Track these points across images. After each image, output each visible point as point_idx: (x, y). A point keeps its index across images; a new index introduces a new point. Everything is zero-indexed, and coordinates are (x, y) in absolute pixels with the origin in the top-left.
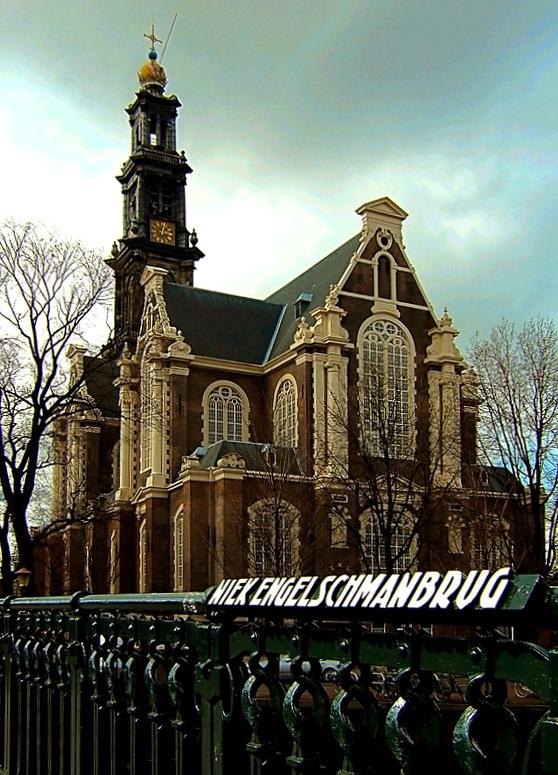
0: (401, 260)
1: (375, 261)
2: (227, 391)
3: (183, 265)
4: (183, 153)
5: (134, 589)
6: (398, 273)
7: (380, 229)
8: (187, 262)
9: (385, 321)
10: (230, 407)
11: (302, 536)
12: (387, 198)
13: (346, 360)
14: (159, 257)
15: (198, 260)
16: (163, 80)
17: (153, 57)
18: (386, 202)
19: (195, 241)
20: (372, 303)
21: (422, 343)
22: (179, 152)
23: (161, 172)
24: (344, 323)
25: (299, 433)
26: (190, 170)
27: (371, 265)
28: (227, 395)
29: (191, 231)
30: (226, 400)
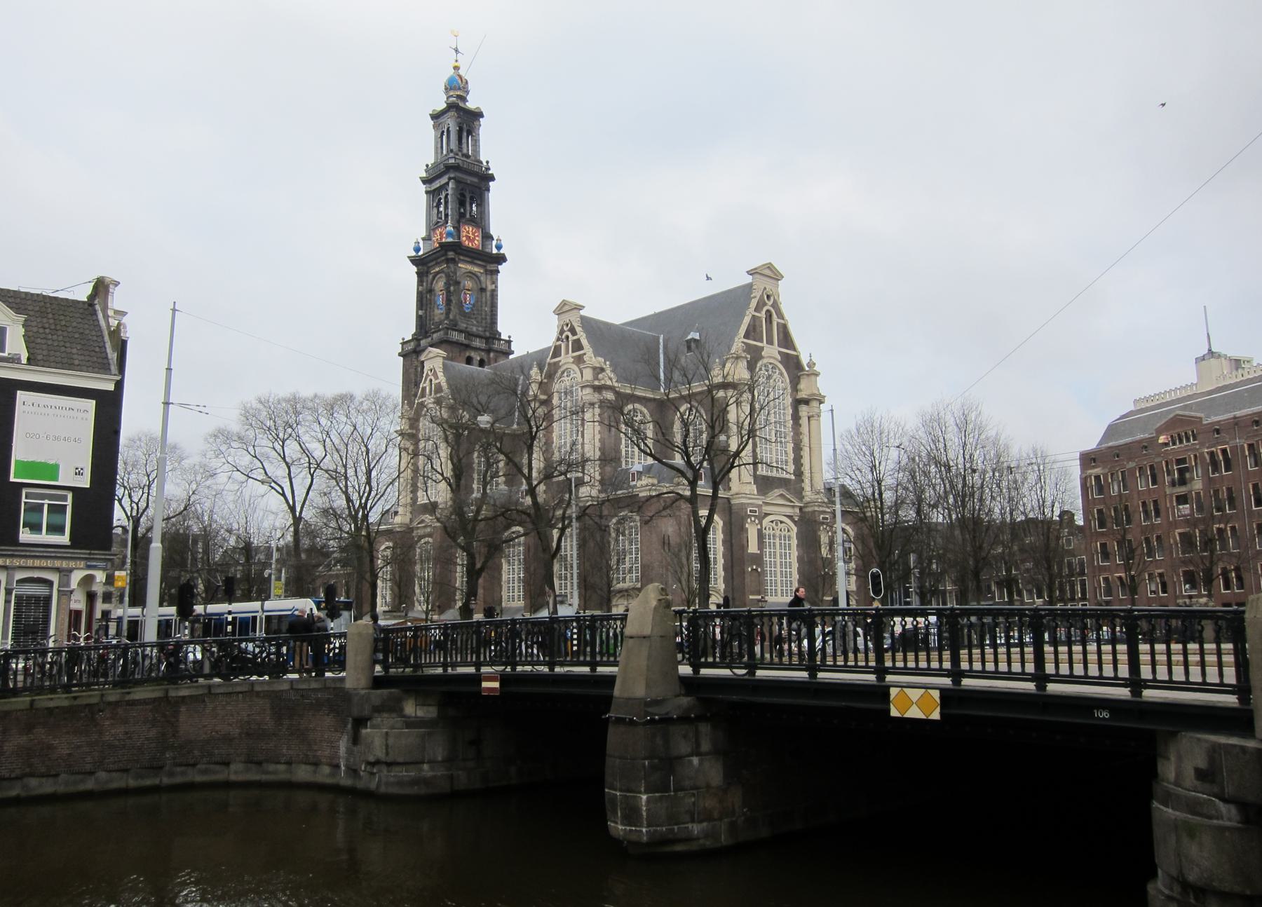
0: (780, 315)
1: (763, 315)
3: (488, 268)
4: (487, 162)
5: (26, 498)
6: (778, 324)
7: (765, 289)
8: (491, 267)
9: (771, 363)
11: (695, 532)
12: (770, 263)
14: (469, 260)
15: (501, 264)
16: (468, 92)
17: (456, 68)
18: (770, 266)
20: (762, 348)
21: (795, 382)
23: (470, 179)
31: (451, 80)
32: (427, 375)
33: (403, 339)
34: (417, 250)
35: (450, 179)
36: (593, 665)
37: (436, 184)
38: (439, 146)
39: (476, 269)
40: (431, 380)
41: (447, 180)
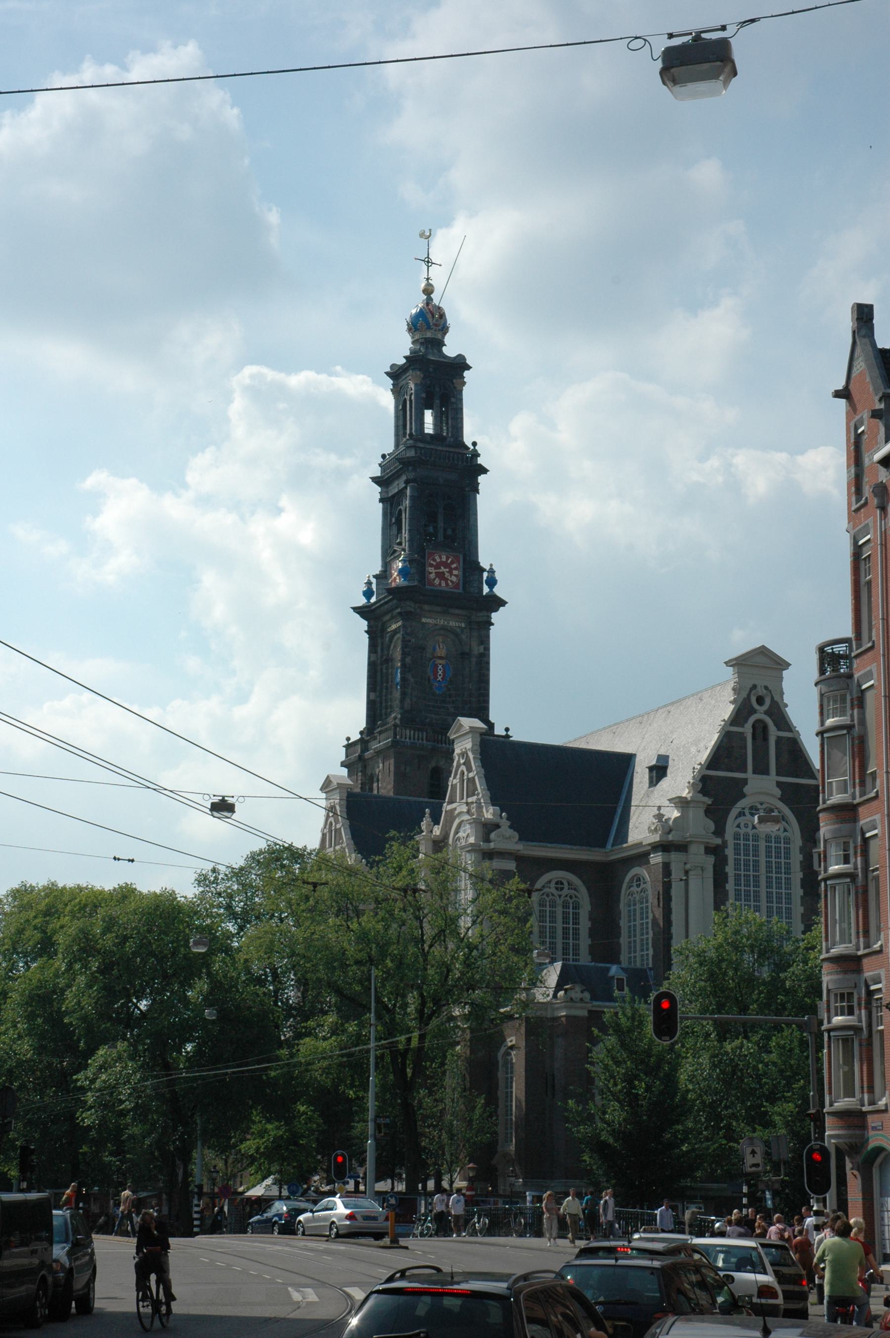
1: (748, 729)
2: (562, 883)
6: (779, 740)
10: (565, 906)
13: (711, 860)
15: (496, 610)
19: (492, 582)
20: (745, 782)
22: (468, 441)
24: (708, 812)
25: (653, 947)
26: (468, 368)
27: (742, 733)
28: (562, 889)
29: (487, 568)
30: (560, 896)
31: (421, 314)
32: (459, 766)
33: (348, 739)
34: (368, 594)
35: (407, 482)
36: (617, 1260)
37: (394, 490)
38: (401, 423)
39: (453, 624)
40: (463, 773)
41: (402, 485)
